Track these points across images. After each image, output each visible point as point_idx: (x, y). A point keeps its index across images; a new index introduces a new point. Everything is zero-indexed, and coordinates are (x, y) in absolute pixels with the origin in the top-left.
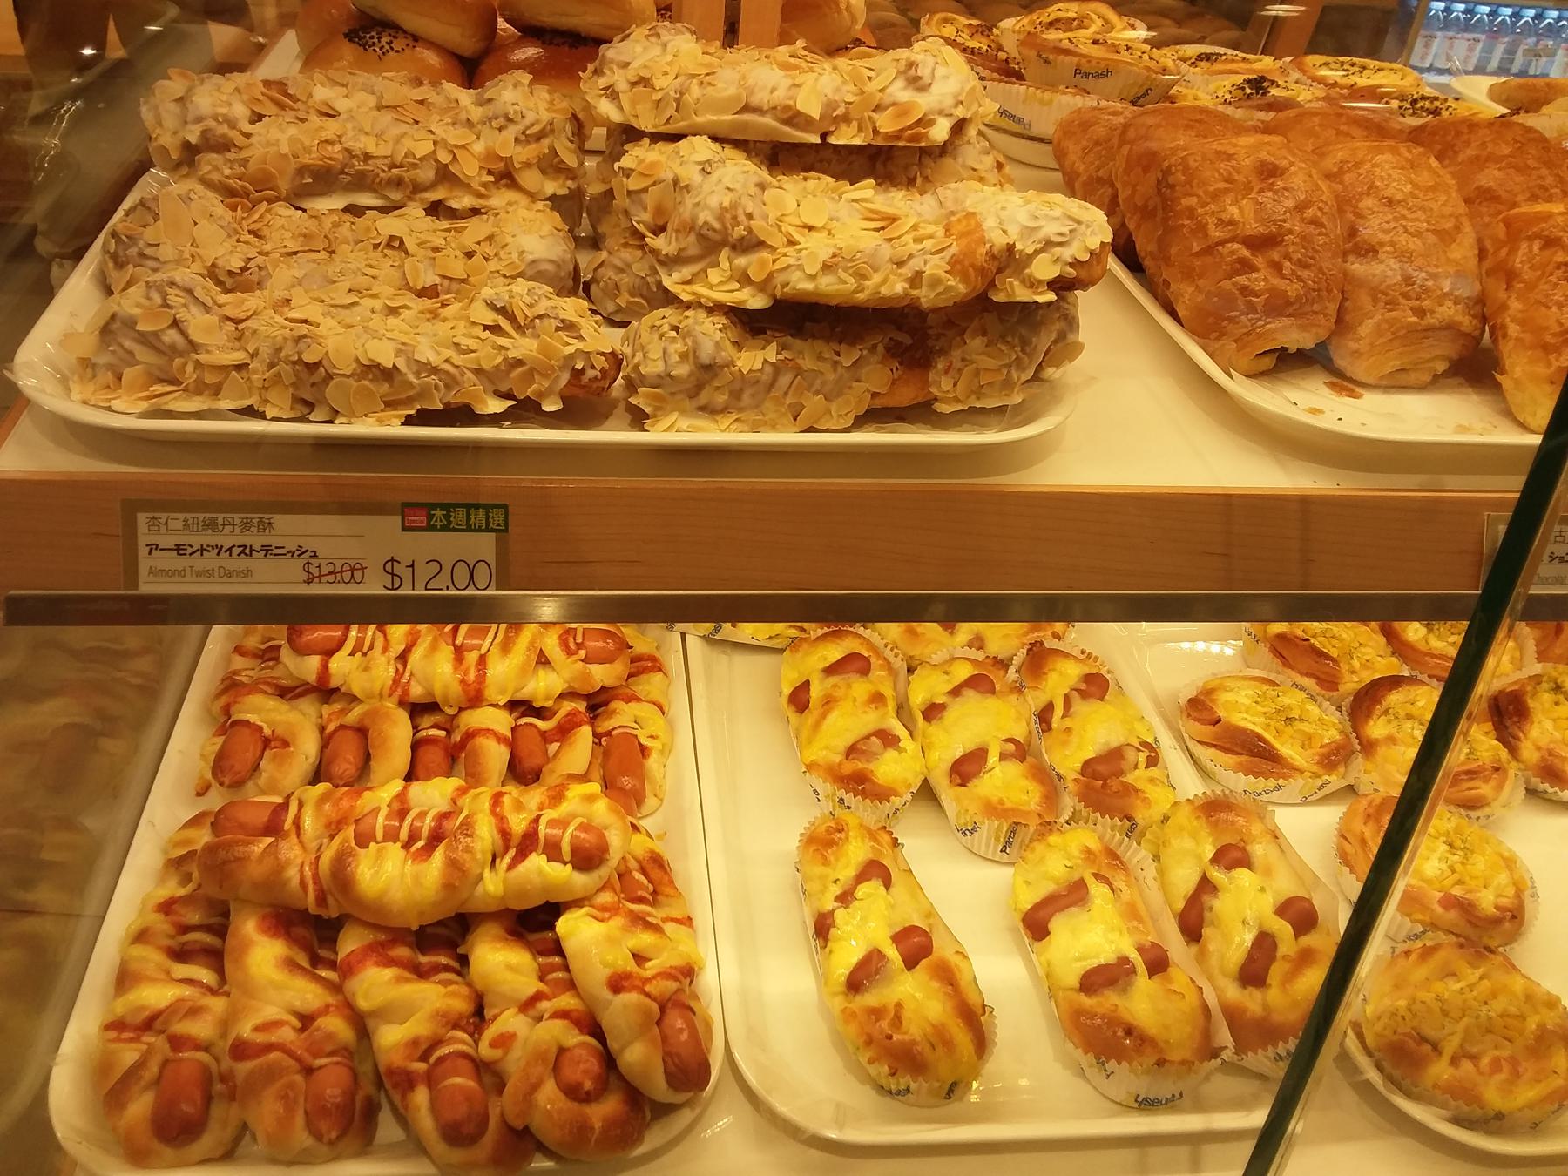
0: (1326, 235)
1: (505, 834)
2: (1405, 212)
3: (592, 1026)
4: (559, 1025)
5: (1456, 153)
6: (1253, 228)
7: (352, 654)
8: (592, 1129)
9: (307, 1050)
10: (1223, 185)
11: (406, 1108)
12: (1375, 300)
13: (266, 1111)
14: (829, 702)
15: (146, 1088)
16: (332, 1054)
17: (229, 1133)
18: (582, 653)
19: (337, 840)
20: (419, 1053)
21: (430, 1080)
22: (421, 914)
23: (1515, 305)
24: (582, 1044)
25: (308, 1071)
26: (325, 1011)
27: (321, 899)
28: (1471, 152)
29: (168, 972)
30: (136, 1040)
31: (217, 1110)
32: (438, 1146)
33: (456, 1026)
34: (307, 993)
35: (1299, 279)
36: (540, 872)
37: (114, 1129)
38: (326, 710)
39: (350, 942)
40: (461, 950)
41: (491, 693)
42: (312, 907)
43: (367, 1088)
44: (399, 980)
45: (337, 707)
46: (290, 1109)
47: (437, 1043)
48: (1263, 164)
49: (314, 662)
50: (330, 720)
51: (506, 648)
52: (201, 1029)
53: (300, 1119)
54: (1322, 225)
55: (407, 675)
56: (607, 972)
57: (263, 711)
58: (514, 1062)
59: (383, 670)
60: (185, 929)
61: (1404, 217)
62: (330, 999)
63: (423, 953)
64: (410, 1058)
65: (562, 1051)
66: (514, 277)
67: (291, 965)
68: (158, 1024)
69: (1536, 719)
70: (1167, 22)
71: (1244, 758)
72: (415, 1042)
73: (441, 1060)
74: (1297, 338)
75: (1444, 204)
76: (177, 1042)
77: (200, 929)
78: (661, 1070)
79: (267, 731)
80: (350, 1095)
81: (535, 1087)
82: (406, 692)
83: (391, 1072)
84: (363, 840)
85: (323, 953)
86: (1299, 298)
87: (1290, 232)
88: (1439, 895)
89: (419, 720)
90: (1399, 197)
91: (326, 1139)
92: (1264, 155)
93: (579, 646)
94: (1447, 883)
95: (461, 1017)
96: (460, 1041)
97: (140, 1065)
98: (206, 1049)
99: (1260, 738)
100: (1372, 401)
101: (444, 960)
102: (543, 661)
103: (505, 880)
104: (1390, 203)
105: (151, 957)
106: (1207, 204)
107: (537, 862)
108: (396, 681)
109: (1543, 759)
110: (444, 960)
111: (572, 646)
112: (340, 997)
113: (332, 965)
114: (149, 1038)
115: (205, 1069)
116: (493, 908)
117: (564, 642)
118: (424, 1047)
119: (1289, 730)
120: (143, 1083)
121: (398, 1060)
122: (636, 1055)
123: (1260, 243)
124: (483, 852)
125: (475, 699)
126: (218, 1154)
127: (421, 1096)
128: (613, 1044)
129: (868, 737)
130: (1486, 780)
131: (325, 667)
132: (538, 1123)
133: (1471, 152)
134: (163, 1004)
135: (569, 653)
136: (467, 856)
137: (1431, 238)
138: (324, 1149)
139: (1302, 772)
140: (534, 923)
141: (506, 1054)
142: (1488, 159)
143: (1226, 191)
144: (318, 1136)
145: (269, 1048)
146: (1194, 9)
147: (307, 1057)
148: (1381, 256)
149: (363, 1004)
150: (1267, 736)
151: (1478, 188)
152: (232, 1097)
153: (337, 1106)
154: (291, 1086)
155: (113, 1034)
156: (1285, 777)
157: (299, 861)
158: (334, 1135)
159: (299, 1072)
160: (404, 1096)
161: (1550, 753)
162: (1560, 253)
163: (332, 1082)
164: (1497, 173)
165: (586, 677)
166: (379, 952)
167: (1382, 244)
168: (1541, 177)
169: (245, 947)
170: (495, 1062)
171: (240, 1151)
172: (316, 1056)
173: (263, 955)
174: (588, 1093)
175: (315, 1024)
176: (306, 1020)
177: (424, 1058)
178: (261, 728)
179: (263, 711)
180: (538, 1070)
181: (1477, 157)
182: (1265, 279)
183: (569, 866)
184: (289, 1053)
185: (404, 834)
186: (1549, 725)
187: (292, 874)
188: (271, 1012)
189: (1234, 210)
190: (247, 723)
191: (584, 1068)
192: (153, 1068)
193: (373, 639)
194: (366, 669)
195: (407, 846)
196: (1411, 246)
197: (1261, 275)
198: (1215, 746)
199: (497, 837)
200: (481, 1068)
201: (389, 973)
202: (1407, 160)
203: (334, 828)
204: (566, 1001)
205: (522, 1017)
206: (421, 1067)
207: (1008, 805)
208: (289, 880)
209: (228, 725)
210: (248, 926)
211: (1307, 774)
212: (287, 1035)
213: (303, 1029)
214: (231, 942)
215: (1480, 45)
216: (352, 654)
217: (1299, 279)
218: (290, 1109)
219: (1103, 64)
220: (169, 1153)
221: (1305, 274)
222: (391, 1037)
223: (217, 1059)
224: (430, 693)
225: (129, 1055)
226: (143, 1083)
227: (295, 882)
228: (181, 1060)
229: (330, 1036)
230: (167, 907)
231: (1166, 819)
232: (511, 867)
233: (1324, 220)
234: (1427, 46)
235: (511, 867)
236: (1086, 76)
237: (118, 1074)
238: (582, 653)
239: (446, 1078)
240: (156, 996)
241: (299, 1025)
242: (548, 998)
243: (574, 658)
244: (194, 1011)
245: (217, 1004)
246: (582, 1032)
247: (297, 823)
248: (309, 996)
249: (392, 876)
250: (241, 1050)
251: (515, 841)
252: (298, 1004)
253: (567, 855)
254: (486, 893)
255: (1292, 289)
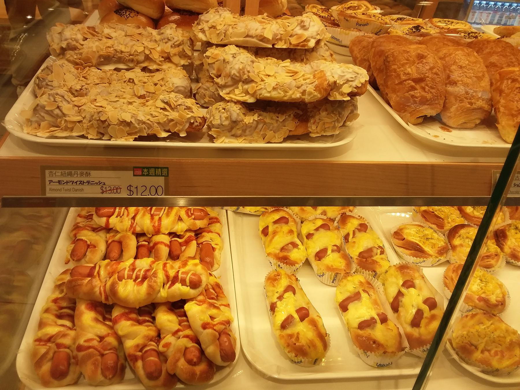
0: (440, 78)
1: (167, 277)
2: (466, 70)
3: (196, 340)
4: (185, 340)
5: (483, 51)
6: (416, 75)
7: (117, 217)
8: (196, 374)
9: (102, 348)
10: (406, 61)
11: (135, 367)
12: (456, 100)
13: (88, 368)
14: (275, 233)
15: (48, 361)
16: (110, 349)
17: (76, 376)
18: (193, 217)
19: (112, 279)
20: (139, 349)
21: (143, 358)
22: (140, 303)
23: (502, 101)
24: (193, 346)
25: (102, 355)
26: (108, 335)
27: (107, 298)
28: (488, 50)
29: (56, 323)
30: (45, 345)
31: (72, 368)
32: (145, 380)
33: (151, 340)
34: (102, 329)
35: (431, 92)
36: (179, 289)
37: (38, 375)
38: (108, 235)
39: (116, 313)
40: (153, 315)
41: (163, 230)
42: (103, 301)
43: (122, 361)
44: (132, 325)
45: (112, 234)
46: (96, 368)
47: (145, 346)
48: (419, 54)
49: (104, 219)
50: (109, 239)
51: (168, 215)
52: (67, 341)
53: (99, 371)
54: (438, 75)
55: (135, 224)
56: (201, 322)
57: (87, 236)
58: (170, 352)
59: (127, 222)
60: (61, 308)
61: (466, 72)
62: (110, 331)
63: (140, 316)
64: (136, 351)
65: (186, 348)
66: (170, 92)
67: (97, 320)
68: (52, 340)
69: (509, 239)
70: (387, 7)
71: (413, 251)
72: (138, 346)
73: (146, 351)
74: (430, 112)
75: (479, 68)
76: (59, 346)
77: (66, 308)
78: (219, 355)
79: (89, 243)
80: (116, 363)
81: (177, 361)
82: (135, 230)
83: (130, 356)
84: (120, 279)
85: (107, 316)
86: (431, 99)
87: (428, 77)
88: (477, 297)
89: (139, 239)
90: (464, 65)
91: (108, 378)
92: (419, 51)
93: (192, 214)
94: (480, 293)
95: (153, 337)
96: (152, 345)
97: (46, 353)
98: (68, 348)
99: (418, 245)
100: (455, 133)
101: (147, 318)
102: (180, 219)
103: (167, 292)
104: (461, 67)
105: (50, 317)
106: (400, 68)
107: (178, 286)
108: (131, 226)
109: (512, 252)
110: (147, 318)
111: (190, 214)
112: (113, 331)
113: (110, 320)
114: (49, 344)
115: (68, 355)
116: (163, 301)
117: (187, 213)
118: (141, 347)
119: (427, 242)
120: (47, 359)
121: (132, 352)
122: (211, 350)
123: (418, 81)
124: (160, 283)
125: (158, 232)
126: (72, 383)
127: (140, 364)
128: (203, 346)
129: (288, 244)
130: (493, 259)
131: (108, 221)
132: (178, 372)
133: (488, 50)
134: (54, 333)
135: (189, 216)
136: (155, 284)
137: (475, 79)
138: (107, 381)
139: (432, 256)
140: (177, 306)
141: (168, 349)
142: (493, 53)
143: (407, 63)
144: (105, 377)
145: (89, 347)
146: (396, 3)
147: (102, 351)
148: (458, 85)
149: (120, 333)
150: (420, 244)
151: (490, 62)
152: (77, 364)
153: (112, 367)
154: (97, 360)
155: (37, 343)
156: (426, 258)
157: (99, 285)
158: (111, 376)
159: (99, 356)
160: (134, 363)
161: (514, 250)
162: (517, 84)
163: (110, 359)
164: (496, 57)
165: (194, 224)
166: (126, 316)
167: (458, 81)
168: (511, 59)
169: (81, 314)
170: (164, 352)
171: (80, 382)
172: (105, 350)
173: (87, 317)
174: (195, 362)
175: (105, 340)
176: (101, 338)
177: (141, 351)
178: (86, 241)
179: (87, 236)
180: (178, 355)
181: (490, 52)
182: (420, 93)
183: (189, 287)
184: (96, 349)
185: (134, 277)
186: (514, 240)
187: (97, 290)
188: (90, 336)
189: (409, 70)
190: (82, 240)
191: (194, 354)
192: (51, 354)
193: (124, 212)
194: (122, 222)
195: (135, 281)
196: (468, 81)
197: (418, 91)
198: (403, 247)
199: (165, 277)
200: (160, 354)
201: (129, 323)
202: (467, 53)
203: (111, 274)
204: (188, 332)
205: (173, 337)
206: (140, 354)
207: (334, 267)
208: (96, 292)
209: (75, 240)
210: (82, 307)
211: (434, 257)
212: (95, 343)
213: (100, 341)
214: (76, 312)
215: (491, 15)
216: (117, 217)
217: (431, 92)
218: (96, 368)
219: (366, 21)
220: (56, 382)
221: (433, 91)
222: (130, 344)
223: (72, 351)
224: (143, 230)
225: (43, 350)
226: (47, 359)
227: (98, 292)
228: (60, 351)
229: (109, 344)
230: (55, 301)
231: (387, 272)
232: (169, 288)
233: (439, 73)
234: (473, 15)
235: (169, 288)
236: (360, 25)
237: (39, 356)
238: (193, 217)
239: (148, 358)
240: (52, 330)
241: (99, 340)
242: (182, 331)
243: (191, 218)
244: (64, 335)
245: (72, 333)
246: (193, 342)
247: (98, 273)
248: (103, 330)
249: (130, 290)
250: (80, 348)
251: (171, 279)
252: (99, 333)
253: (188, 284)
254: (161, 296)
255: (429, 96)
